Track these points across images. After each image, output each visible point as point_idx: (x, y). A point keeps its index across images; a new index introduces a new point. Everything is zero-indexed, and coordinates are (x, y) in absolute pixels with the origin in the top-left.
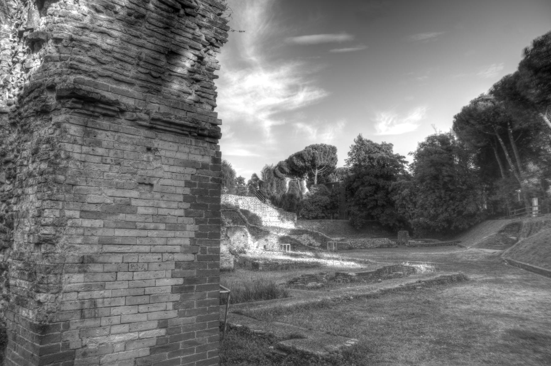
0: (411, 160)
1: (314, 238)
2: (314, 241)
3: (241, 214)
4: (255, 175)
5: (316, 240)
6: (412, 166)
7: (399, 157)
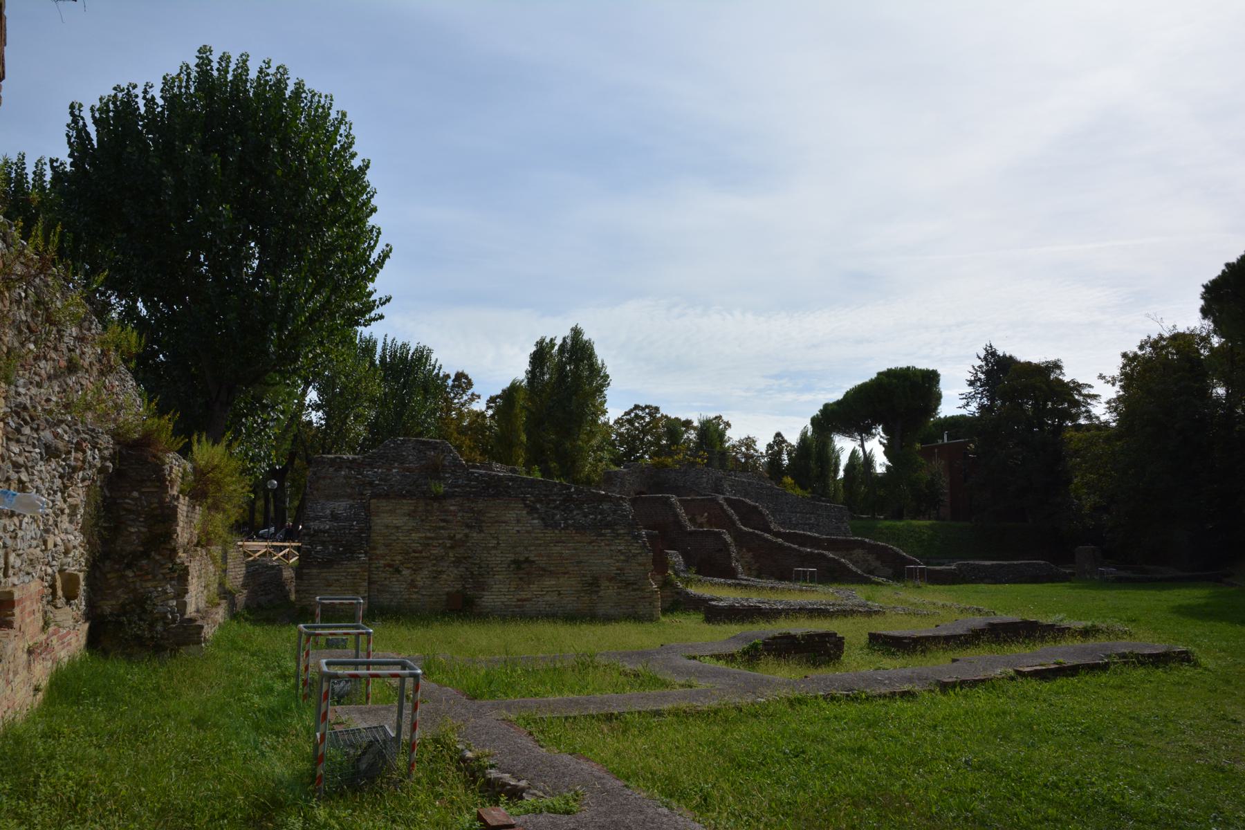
0: (1111, 392)
2: (878, 564)
6: (1112, 405)
7: (1078, 387)
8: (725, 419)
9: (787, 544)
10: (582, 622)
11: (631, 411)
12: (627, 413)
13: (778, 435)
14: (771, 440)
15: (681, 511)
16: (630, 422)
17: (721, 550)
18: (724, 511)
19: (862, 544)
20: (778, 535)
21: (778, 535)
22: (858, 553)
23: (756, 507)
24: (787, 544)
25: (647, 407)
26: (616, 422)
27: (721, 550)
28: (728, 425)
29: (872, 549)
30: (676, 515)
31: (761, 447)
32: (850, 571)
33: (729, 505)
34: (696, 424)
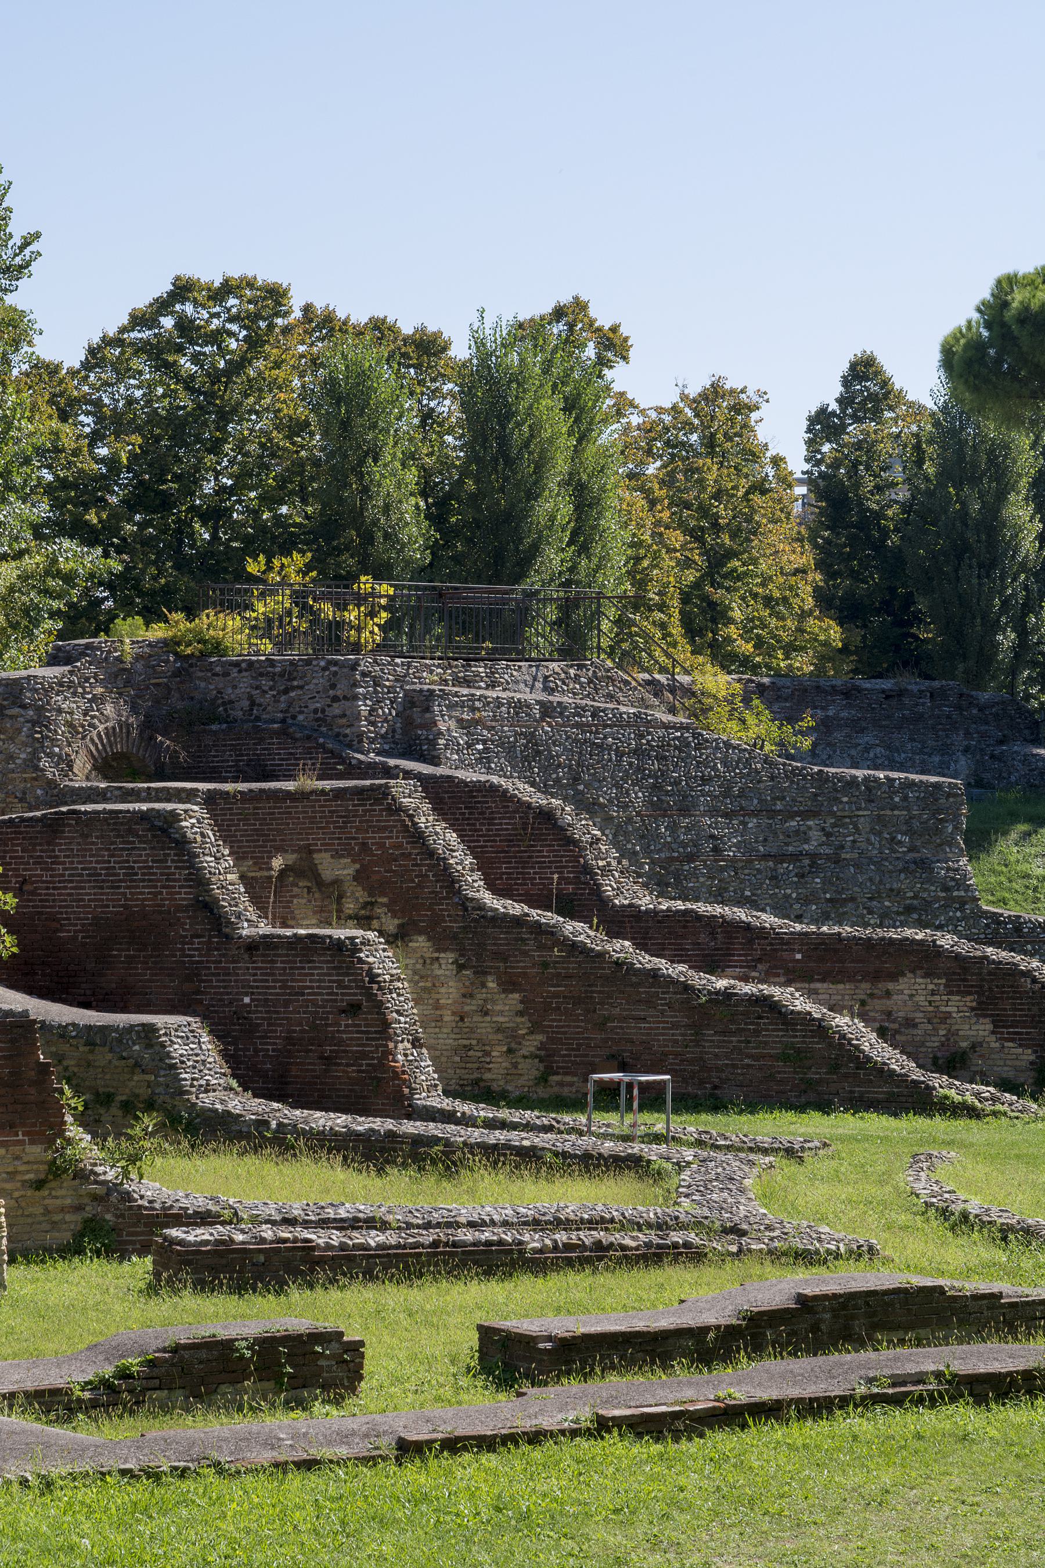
1: (980, 1010)
2: (982, 1029)
3: (426, 819)
4: (862, 369)
5: (998, 1023)
8: (603, 316)
9: (646, 961)
10: (867, 1110)
11: (163, 305)
12: (138, 320)
13: (862, 369)
14: (828, 393)
15: (222, 869)
16: (158, 353)
17: (354, 1009)
18: (418, 837)
19: (926, 958)
20: (621, 922)
21: (621, 922)
22: (912, 992)
23: (547, 816)
24: (646, 961)
25: (228, 288)
26: (95, 357)
27: (354, 1009)
28: (613, 345)
29: (961, 973)
30: (199, 881)
31: (783, 436)
32: (861, 1062)
33: (440, 808)
34: (461, 350)
